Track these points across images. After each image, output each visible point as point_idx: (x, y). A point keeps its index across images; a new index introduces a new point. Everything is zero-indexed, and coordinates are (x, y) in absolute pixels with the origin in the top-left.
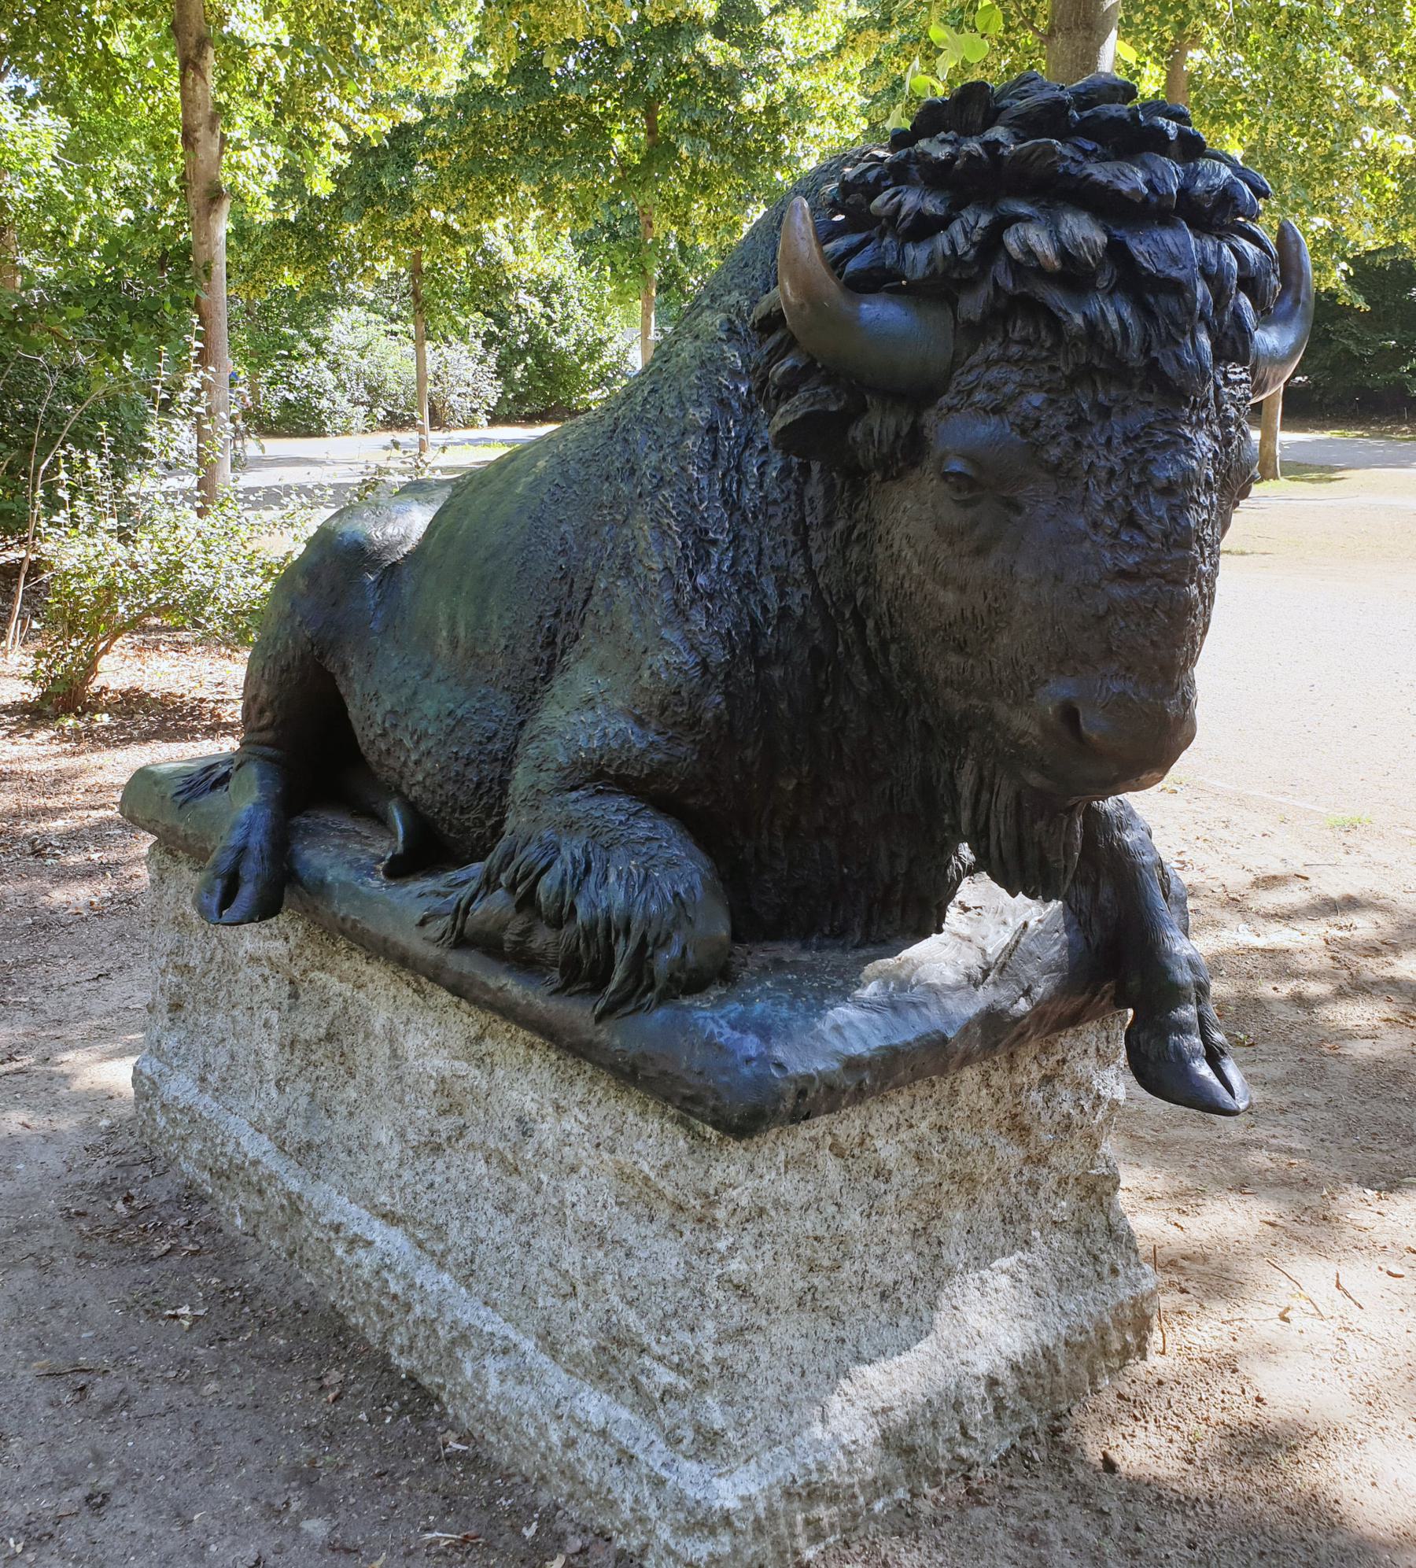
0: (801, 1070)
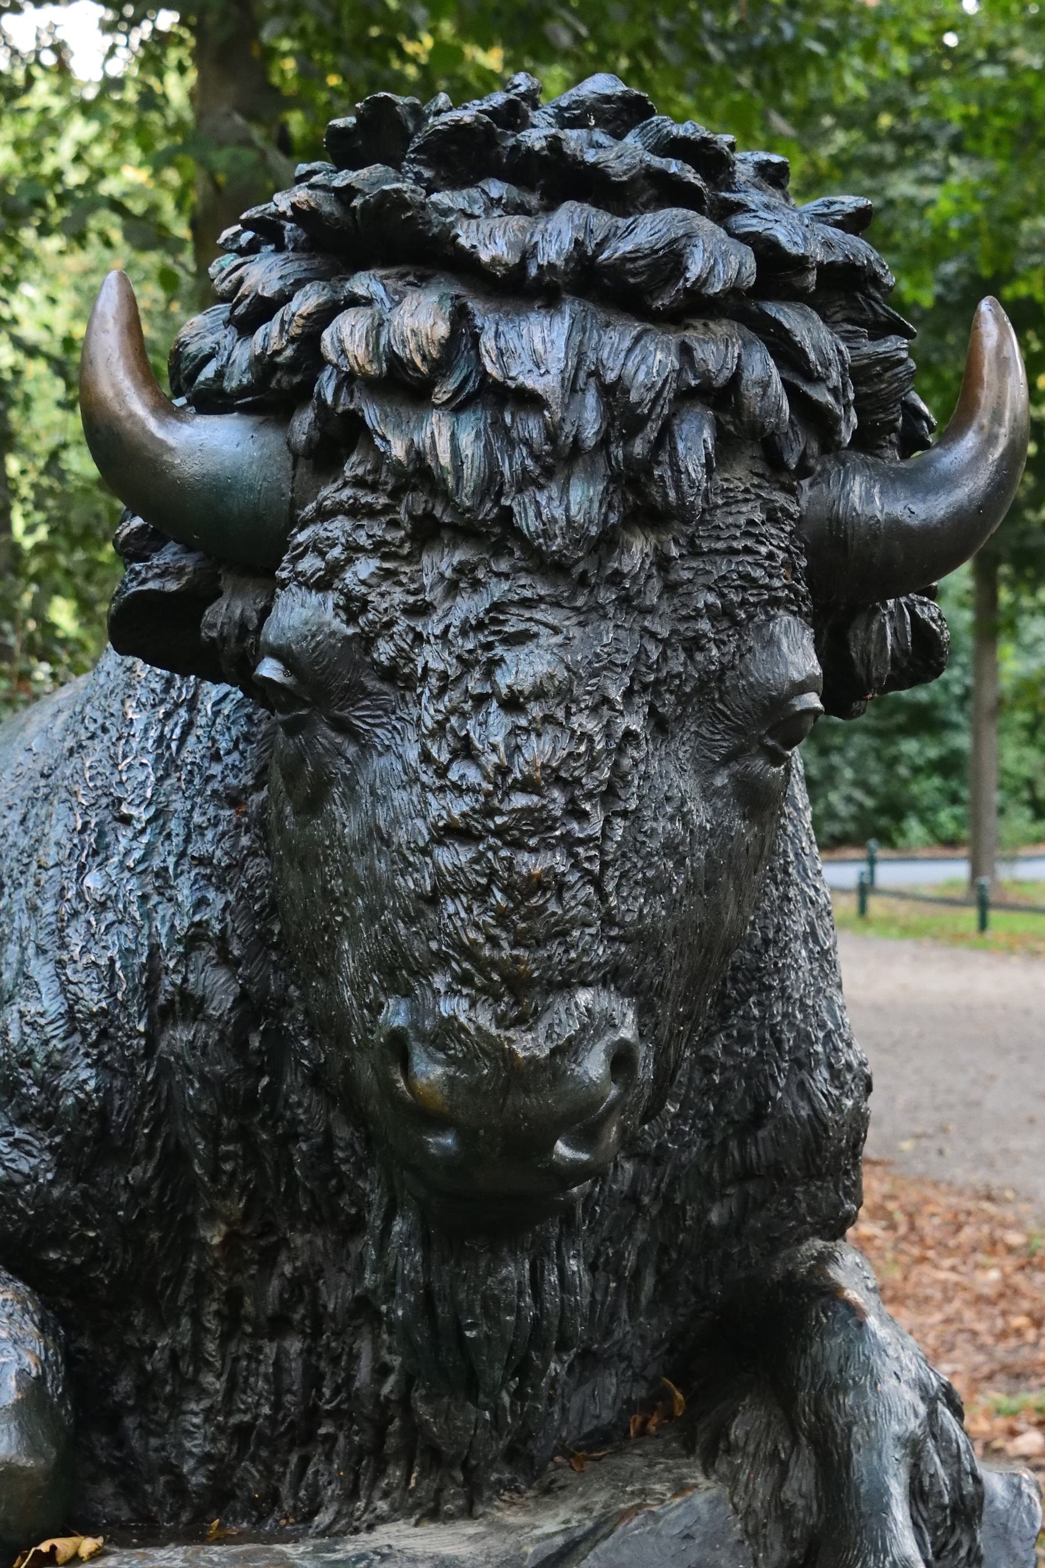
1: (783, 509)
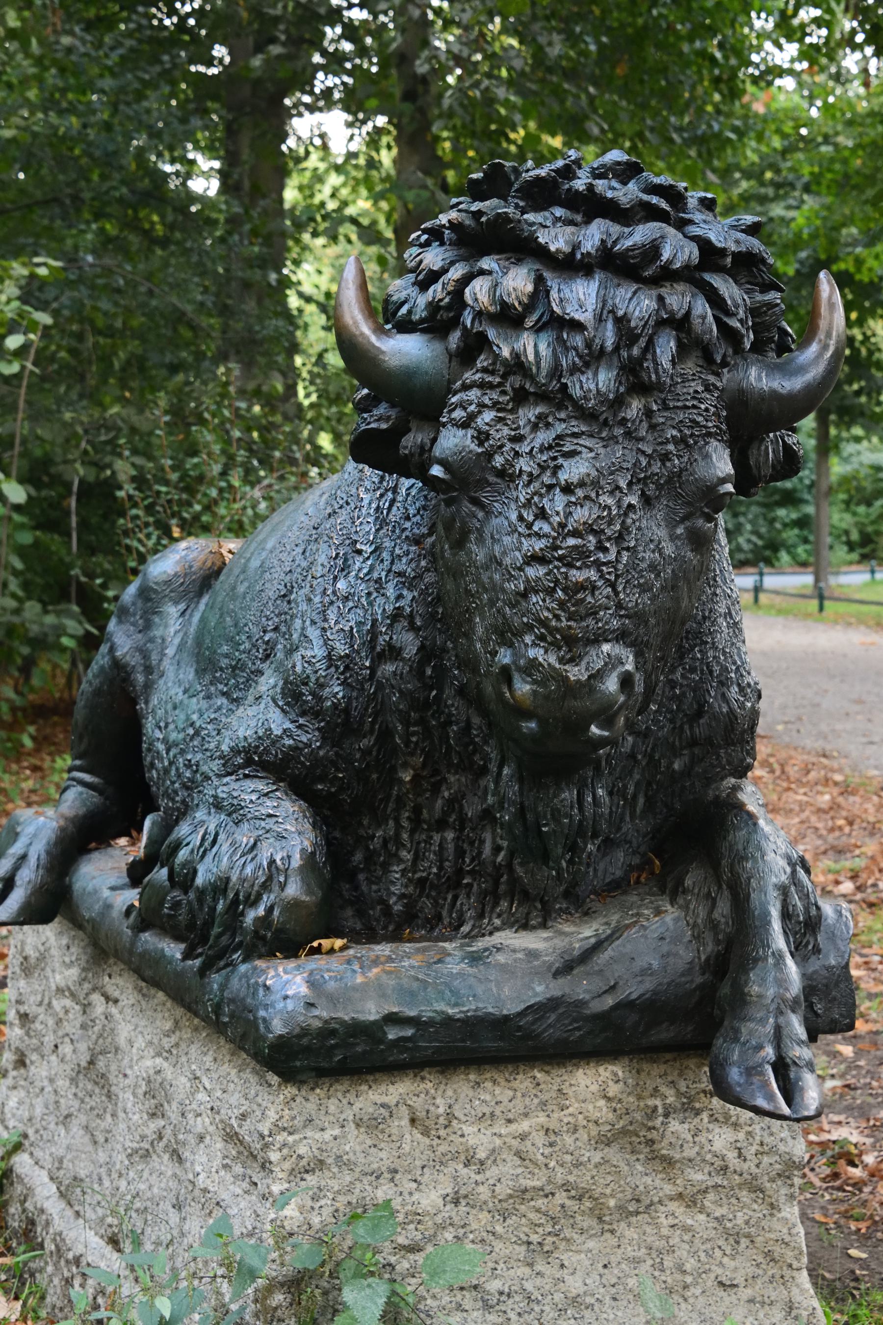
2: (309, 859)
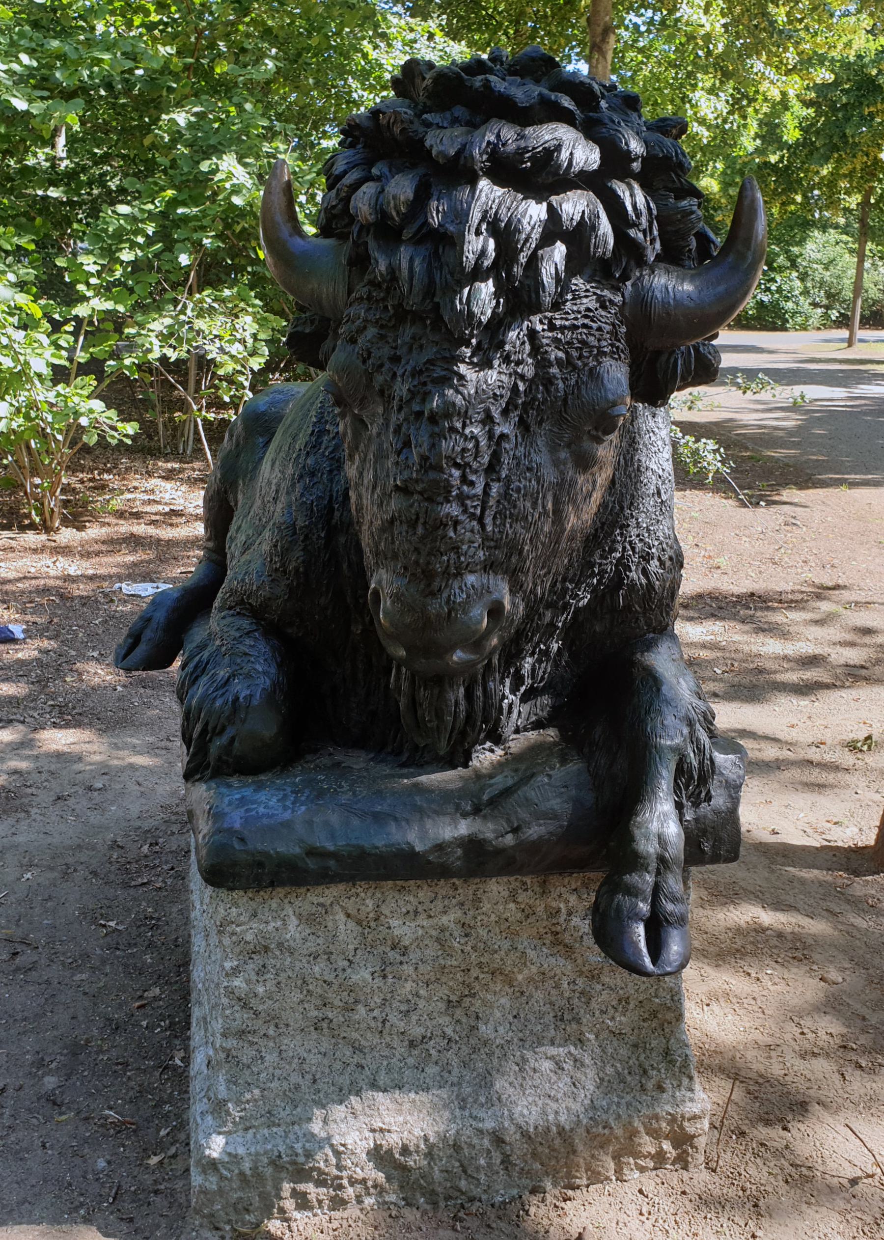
0: (259, 847)
1: (611, 301)
2: (270, 697)
